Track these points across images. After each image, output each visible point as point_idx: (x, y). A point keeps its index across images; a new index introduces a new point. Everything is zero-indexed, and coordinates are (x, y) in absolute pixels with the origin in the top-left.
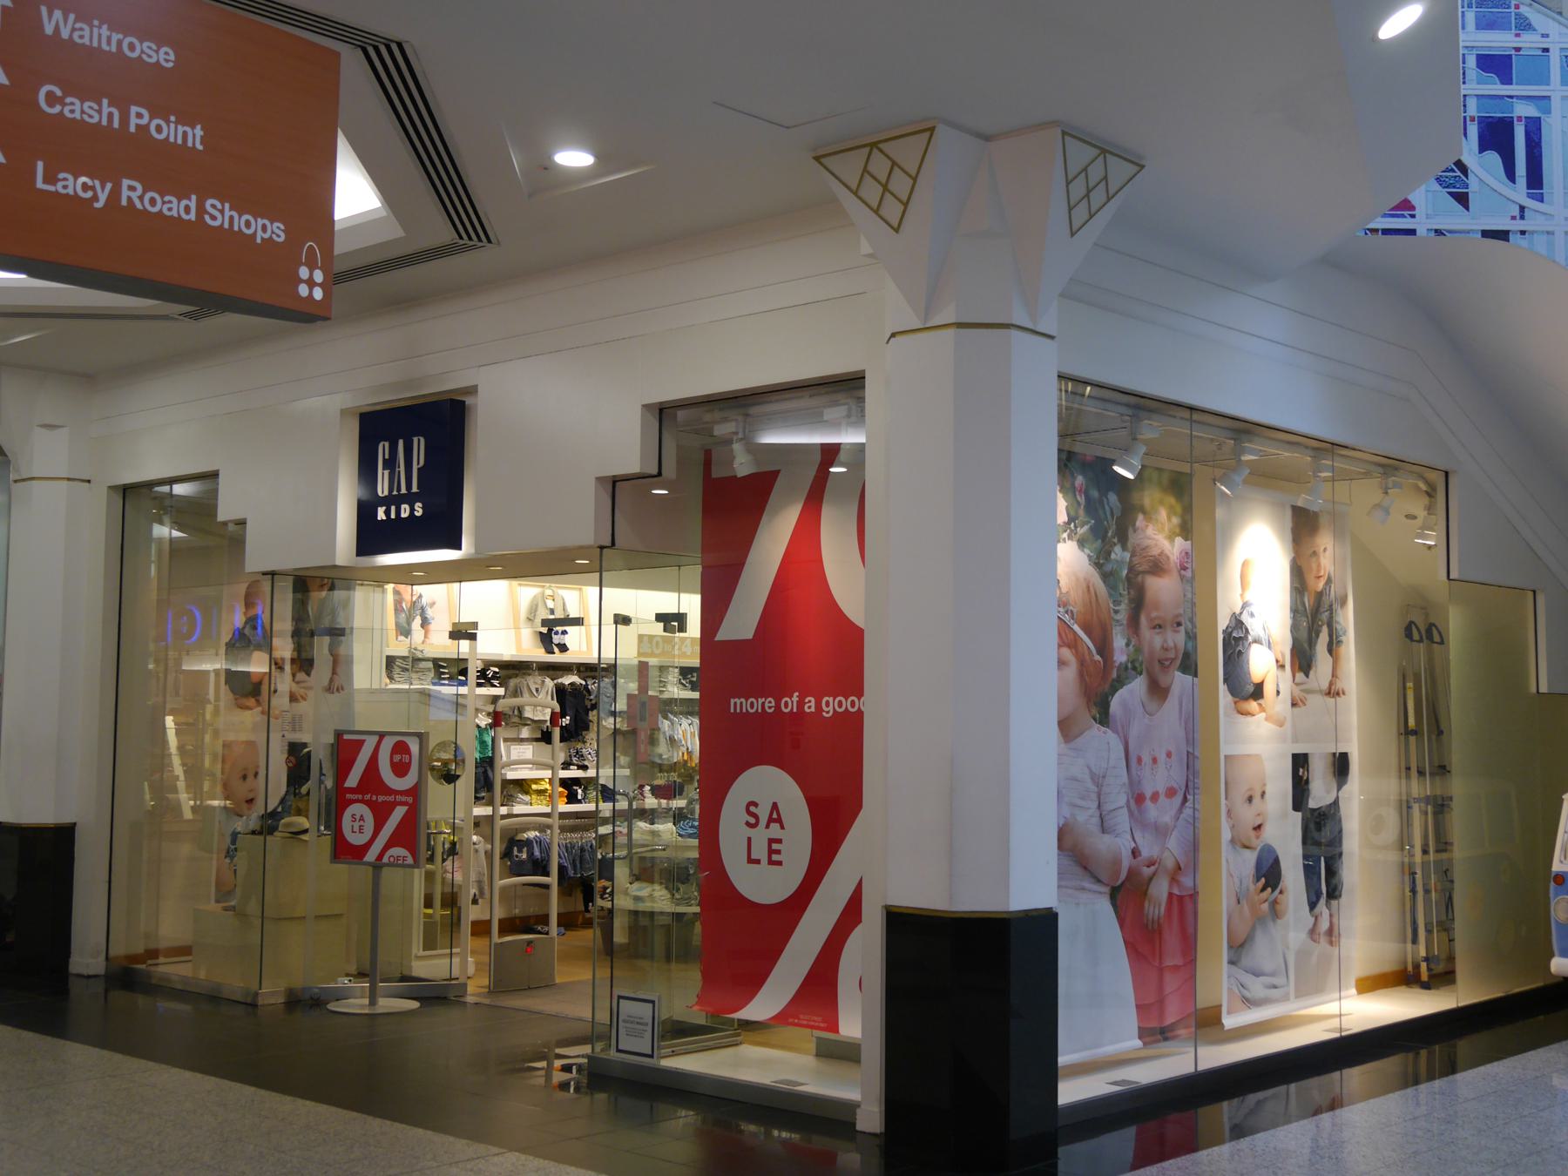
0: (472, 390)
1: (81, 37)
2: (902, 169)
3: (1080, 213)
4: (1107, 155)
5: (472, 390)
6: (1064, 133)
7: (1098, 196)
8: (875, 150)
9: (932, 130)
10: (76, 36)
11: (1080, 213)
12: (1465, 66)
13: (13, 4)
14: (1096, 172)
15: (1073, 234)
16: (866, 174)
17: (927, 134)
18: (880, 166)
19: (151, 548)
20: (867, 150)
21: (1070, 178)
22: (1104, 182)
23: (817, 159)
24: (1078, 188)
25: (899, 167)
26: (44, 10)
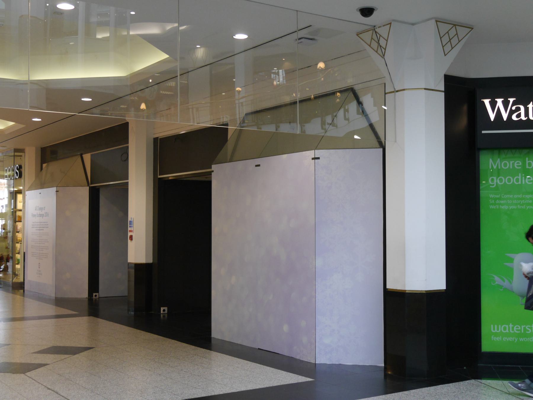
0: (133, 233)
1: (519, 116)
2: (382, 37)
3: (448, 47)
4: (456, 26)
5: (133, 233)
6: (436, 21)
7: (454, 41)
8: (454, 27)
9: (390, 24)
10: (514, 117)
11: (448, 47)
12: (297, 31)
13: (169, 55)
14: (453, 32)
15: (445, 55)
16: (372, 40)
17: (389, 25)
18: (453, 32)
19: (183, 26)
20: (453, 26)
21: (456, 35)
22: (456, 35)
23: (357, 35)
24: (446, 39)
25: (382, 37)
26: (490, 206)
